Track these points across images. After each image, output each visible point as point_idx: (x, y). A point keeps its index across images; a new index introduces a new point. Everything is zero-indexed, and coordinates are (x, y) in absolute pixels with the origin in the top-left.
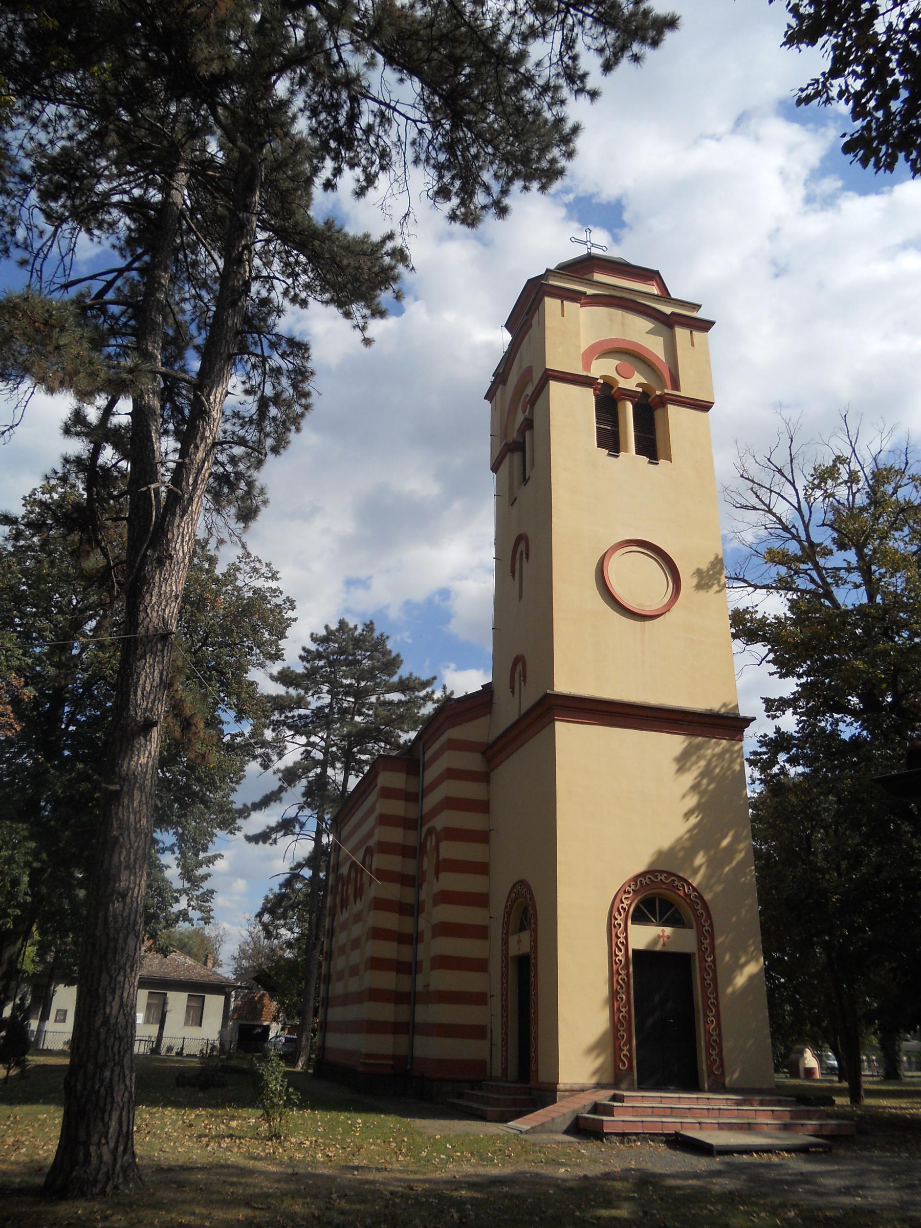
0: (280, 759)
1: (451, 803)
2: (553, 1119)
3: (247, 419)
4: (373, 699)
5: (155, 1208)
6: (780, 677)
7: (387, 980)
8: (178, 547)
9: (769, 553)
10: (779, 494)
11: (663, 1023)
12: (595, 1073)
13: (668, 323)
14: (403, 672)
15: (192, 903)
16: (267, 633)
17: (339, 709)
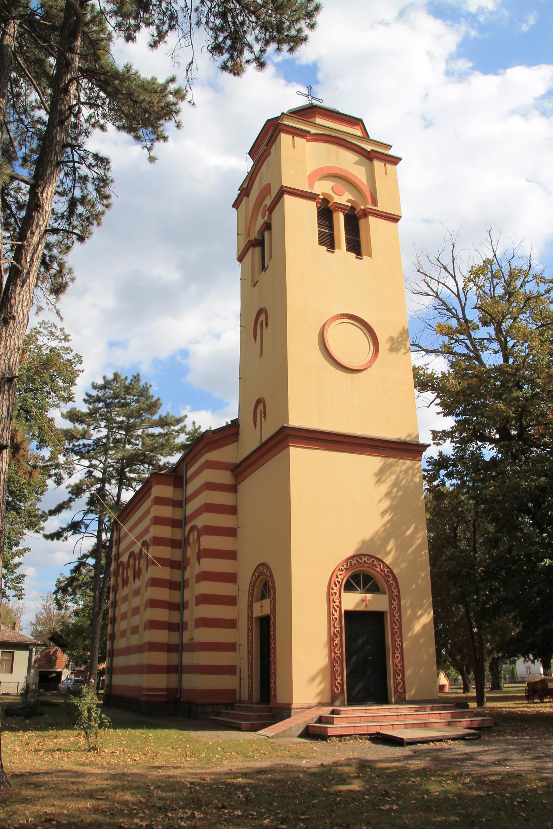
0: (70, 477)
1: (209, 508)
2: (291, 728)
3: (59, 215)
4: (139, 432)
5: (23, 803)
6: (444, 416)
7: (161, 636)
8: (19, 310)
9: (439, 327)
10: (444, 284)
11: (366, 660)
12: (319, 694)
13: (369, 156)
14: (162, 412)
15: (8, 584)
16: (61, 382)
17: (114, 439)
